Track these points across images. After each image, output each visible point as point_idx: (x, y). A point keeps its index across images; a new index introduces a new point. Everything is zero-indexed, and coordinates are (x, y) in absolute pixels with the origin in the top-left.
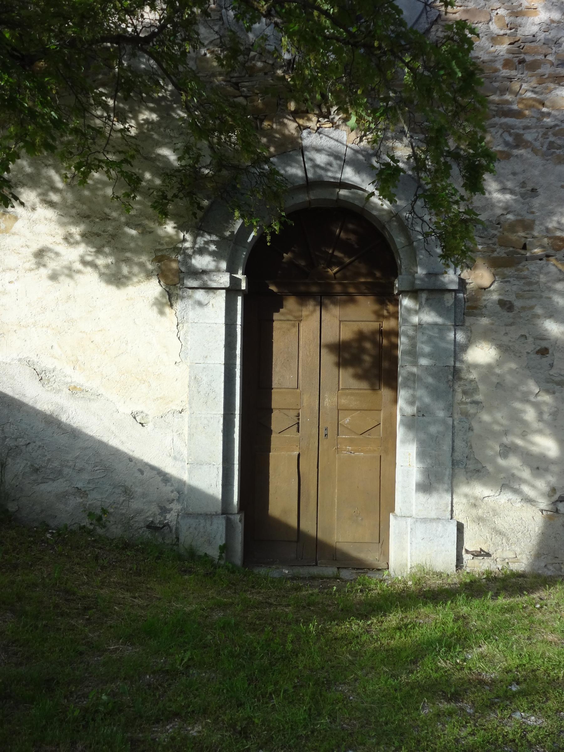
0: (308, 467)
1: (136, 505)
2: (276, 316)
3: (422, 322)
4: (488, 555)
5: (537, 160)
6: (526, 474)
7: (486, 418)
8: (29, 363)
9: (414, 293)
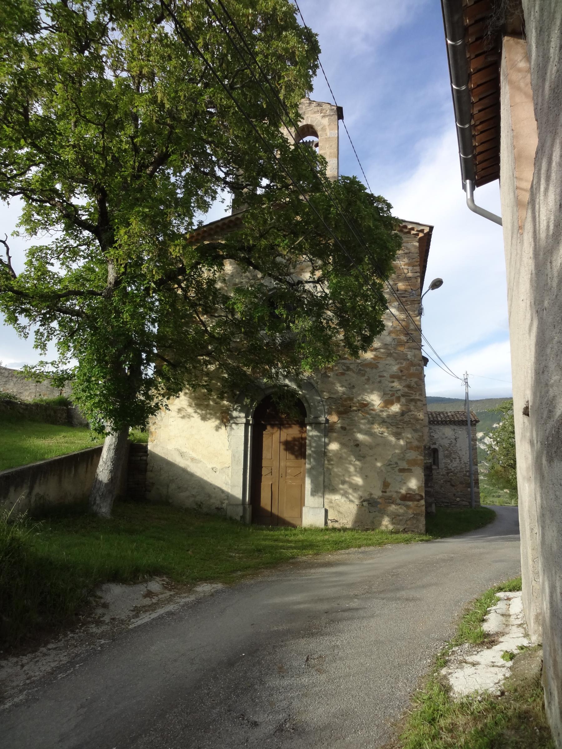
0: (275, 489)
1: (212, 501)
2: (264, 432)
3: (470, 398)
4: (337, 521)
5: (354, 375)
6: (350, 491)
7: (335, 470)
8: (178, 450)
9: (310, 424)
